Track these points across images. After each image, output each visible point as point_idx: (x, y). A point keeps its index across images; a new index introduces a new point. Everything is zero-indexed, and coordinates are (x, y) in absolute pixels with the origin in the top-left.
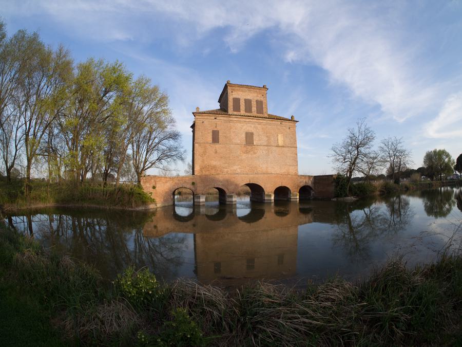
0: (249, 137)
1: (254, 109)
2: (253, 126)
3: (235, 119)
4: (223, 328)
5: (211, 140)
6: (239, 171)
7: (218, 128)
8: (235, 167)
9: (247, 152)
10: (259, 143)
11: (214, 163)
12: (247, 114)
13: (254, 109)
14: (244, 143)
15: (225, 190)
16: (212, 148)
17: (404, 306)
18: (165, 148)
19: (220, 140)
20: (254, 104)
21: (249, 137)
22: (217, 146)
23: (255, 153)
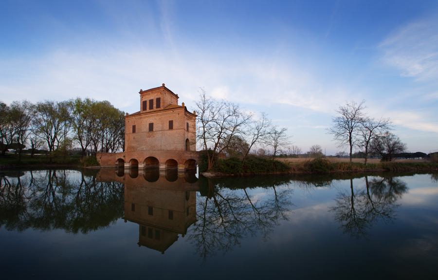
0: (151, 126)
1: (155, 105)
2: (153, 118)
3: (144, 116)
4: (24, 129)
5: (168, 127)
6: (145, 149)
7: (136, 124)
8: (143, 147)
9: (149, 137)
10: (157, 129)
11: (133, 145)
12: (150, 111)
13: (155, 105)
14: (148, 130)
15: (138, 160)
16: (132, 136)
17: (127, 188)
18: (226, 136)
19: (174, 128)
20: (155, 102)
21: (151, 126)
22: (134, 135)
23: (154, 137)
